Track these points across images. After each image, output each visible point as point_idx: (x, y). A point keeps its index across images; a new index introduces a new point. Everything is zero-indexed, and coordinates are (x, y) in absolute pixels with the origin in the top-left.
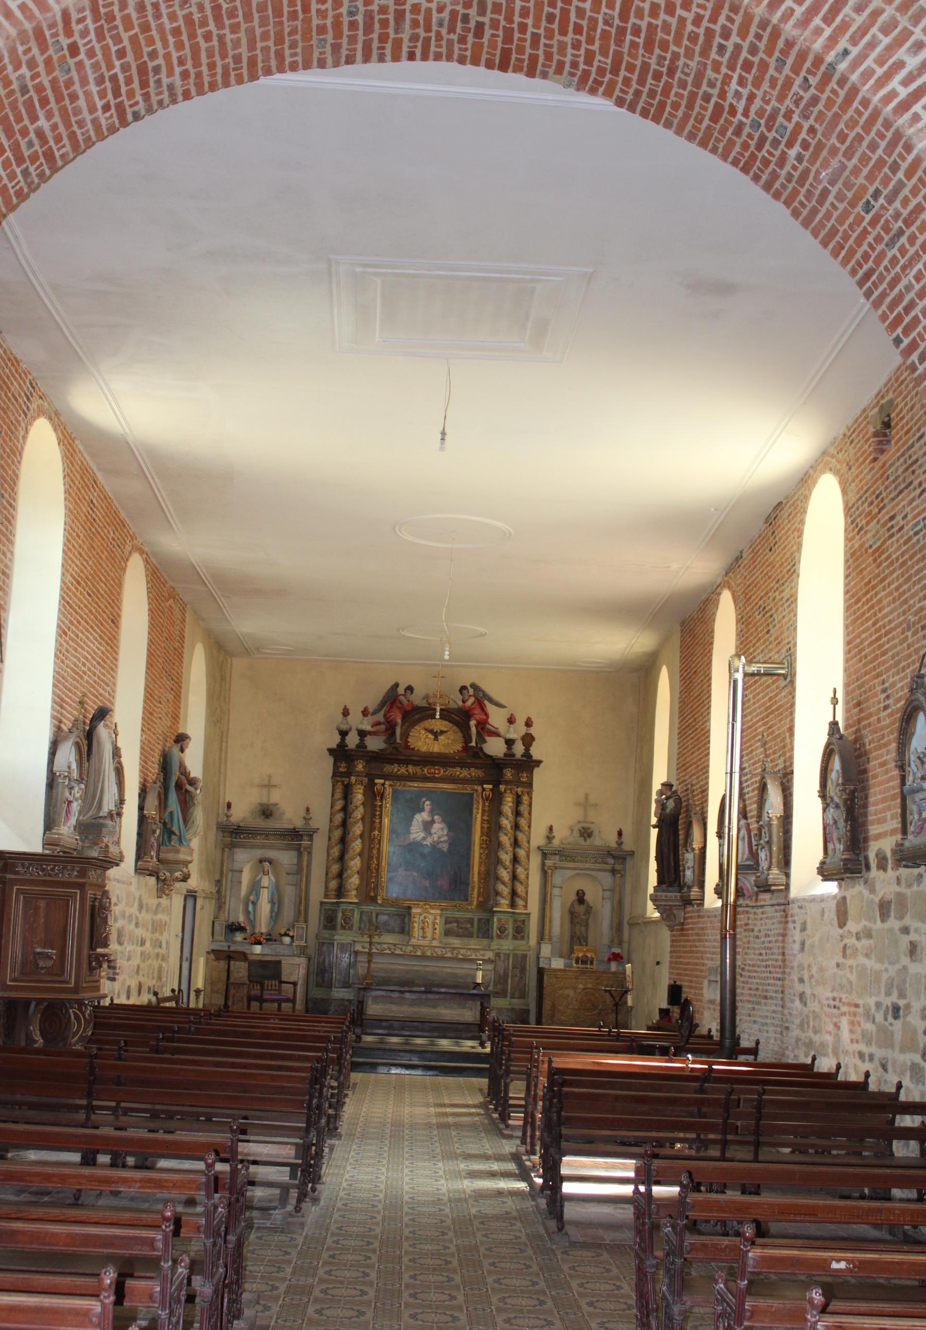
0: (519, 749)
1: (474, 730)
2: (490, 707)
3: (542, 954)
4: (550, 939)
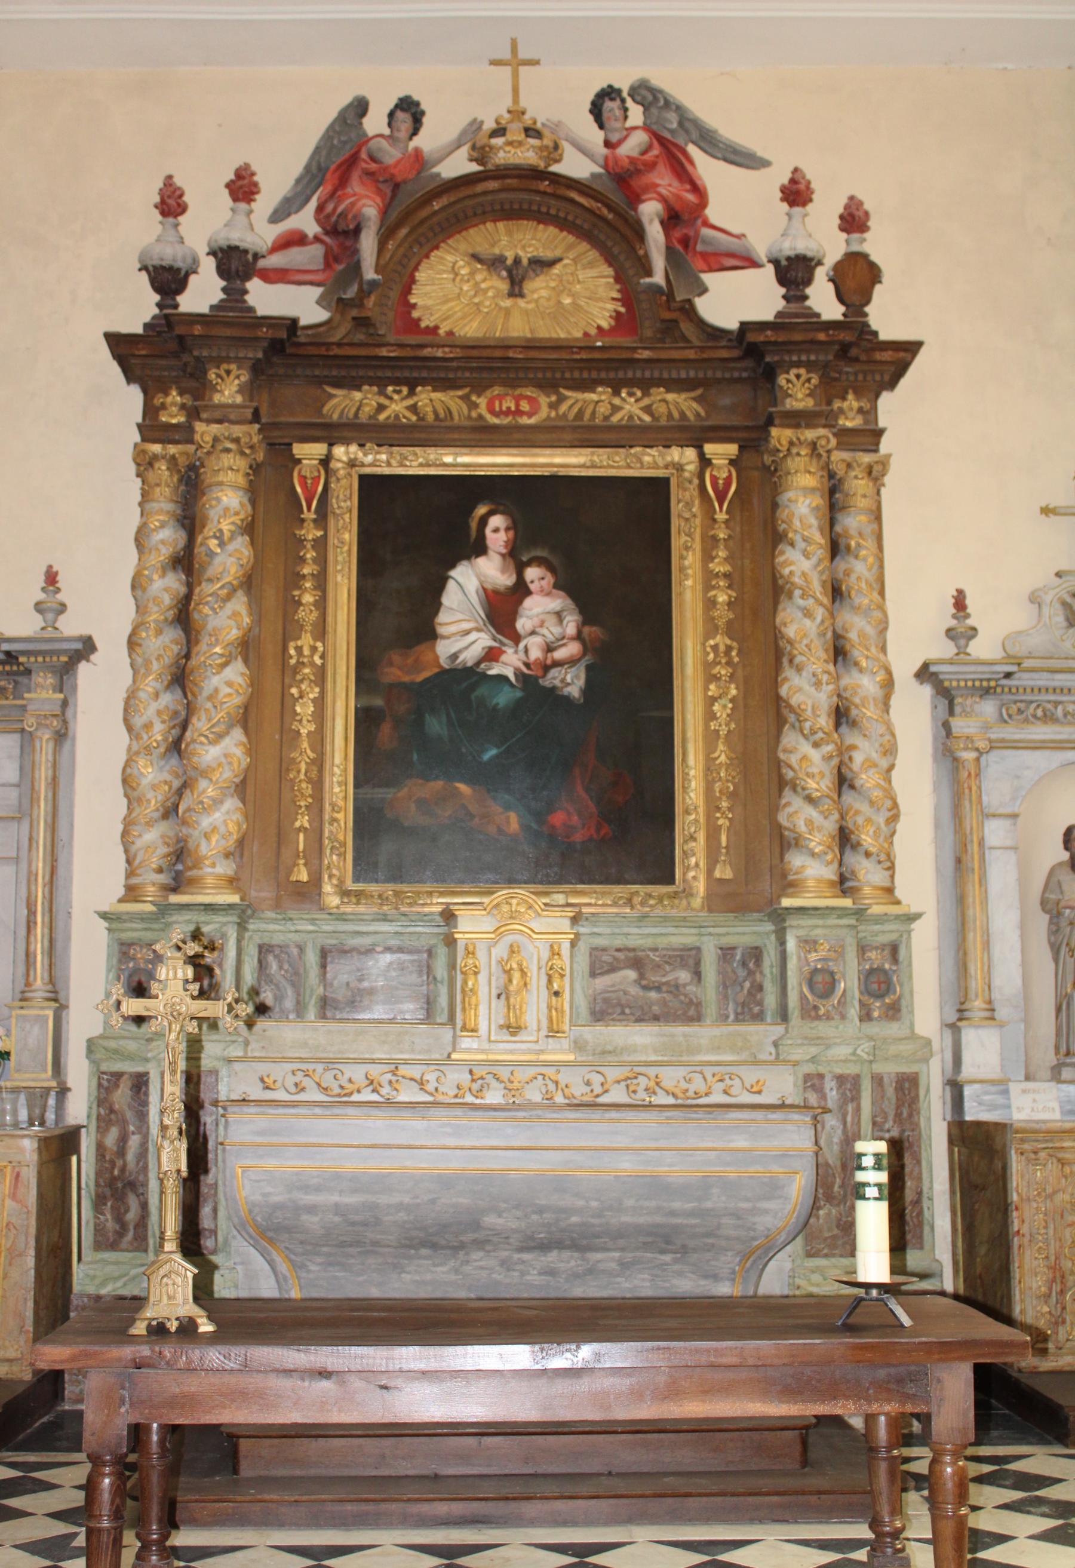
0: (824, 301)
1: (655, 233)
2: (707, 168)
3: (968, 1071)
4: (990, 1014)
